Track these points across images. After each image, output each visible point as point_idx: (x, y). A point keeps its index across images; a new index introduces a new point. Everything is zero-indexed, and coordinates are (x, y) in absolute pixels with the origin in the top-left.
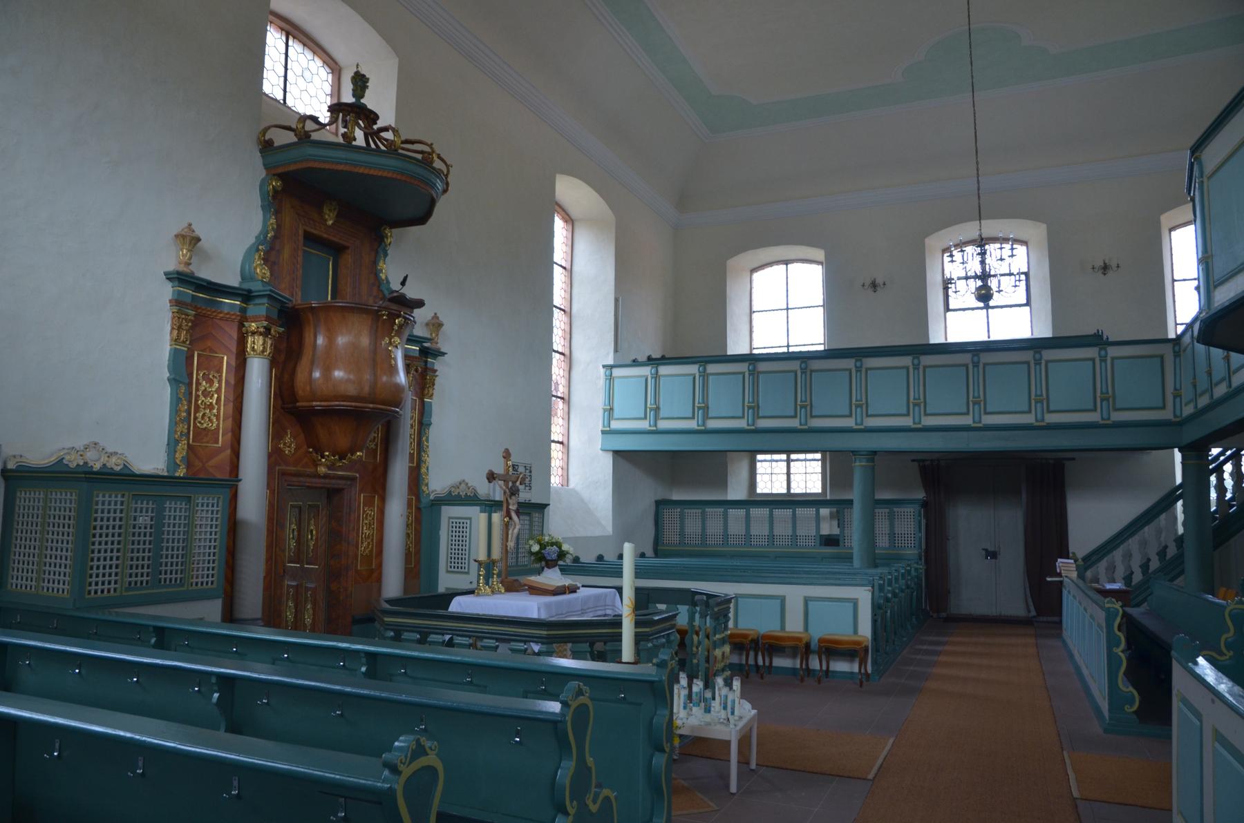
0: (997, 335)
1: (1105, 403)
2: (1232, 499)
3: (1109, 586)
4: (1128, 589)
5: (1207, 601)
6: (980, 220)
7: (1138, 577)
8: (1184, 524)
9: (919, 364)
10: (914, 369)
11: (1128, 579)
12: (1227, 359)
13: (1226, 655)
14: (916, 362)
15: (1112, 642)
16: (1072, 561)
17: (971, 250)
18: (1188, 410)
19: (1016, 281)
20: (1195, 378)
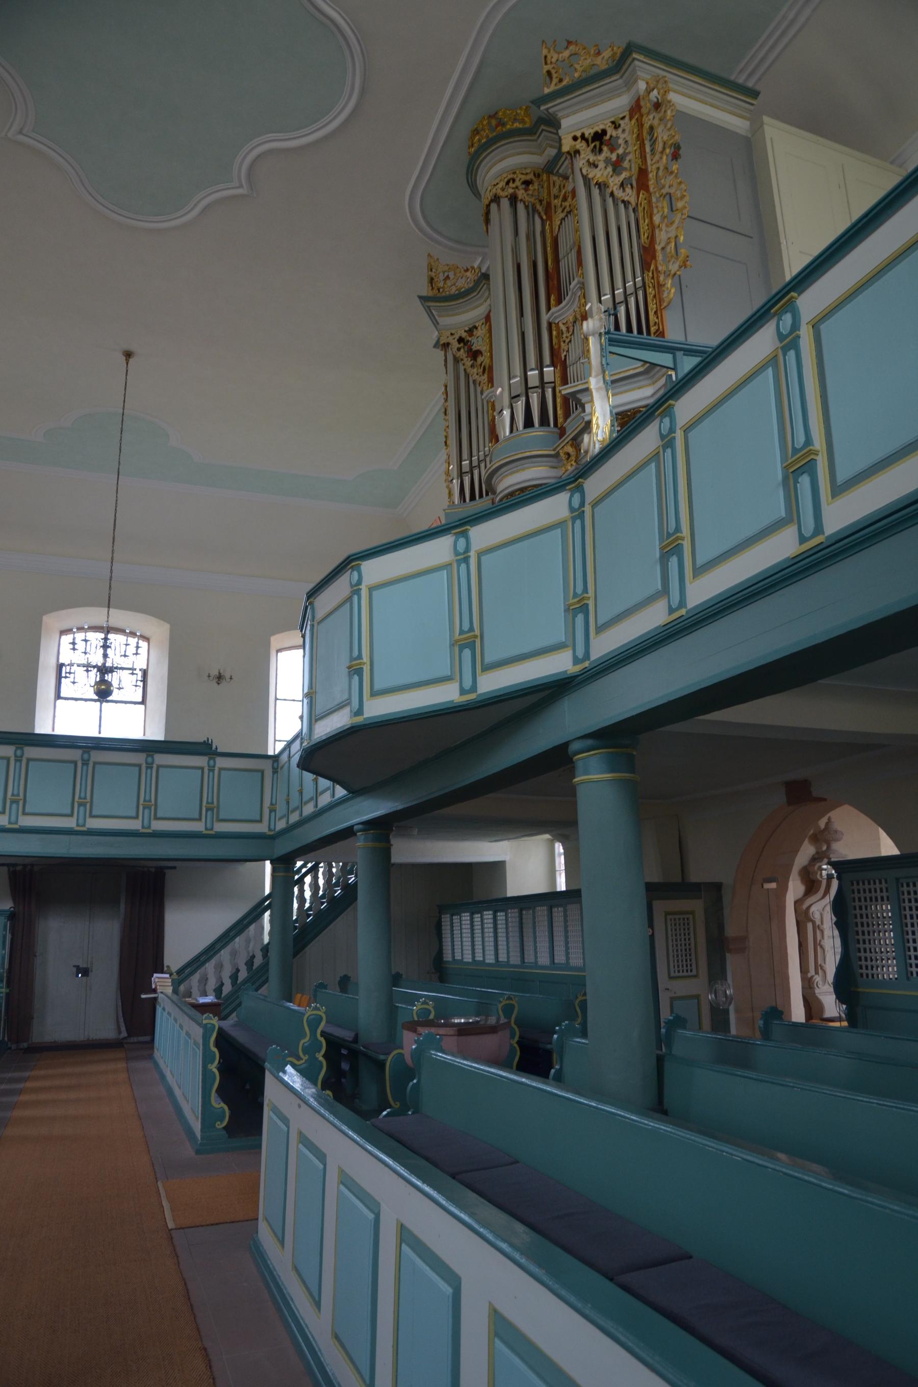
0: (109, 732)
1: (209, 813)
2: (310, 909)
3: (202, 1000)
4: (220, 1001)
5: (288, 1008)
6: (109, 607)
7: (227, 988)
8: (270, 934)
9: (22, 756)
10: (16, 761)
11: (218, 991)
12: (316, 781)
13: (302, 1059)
14: (19, 753)
15: (207, 1058)
16: (168, 976)
17: (96, 638)
18: (281, 825)
19: (137, 681)
20: (288, 795)
